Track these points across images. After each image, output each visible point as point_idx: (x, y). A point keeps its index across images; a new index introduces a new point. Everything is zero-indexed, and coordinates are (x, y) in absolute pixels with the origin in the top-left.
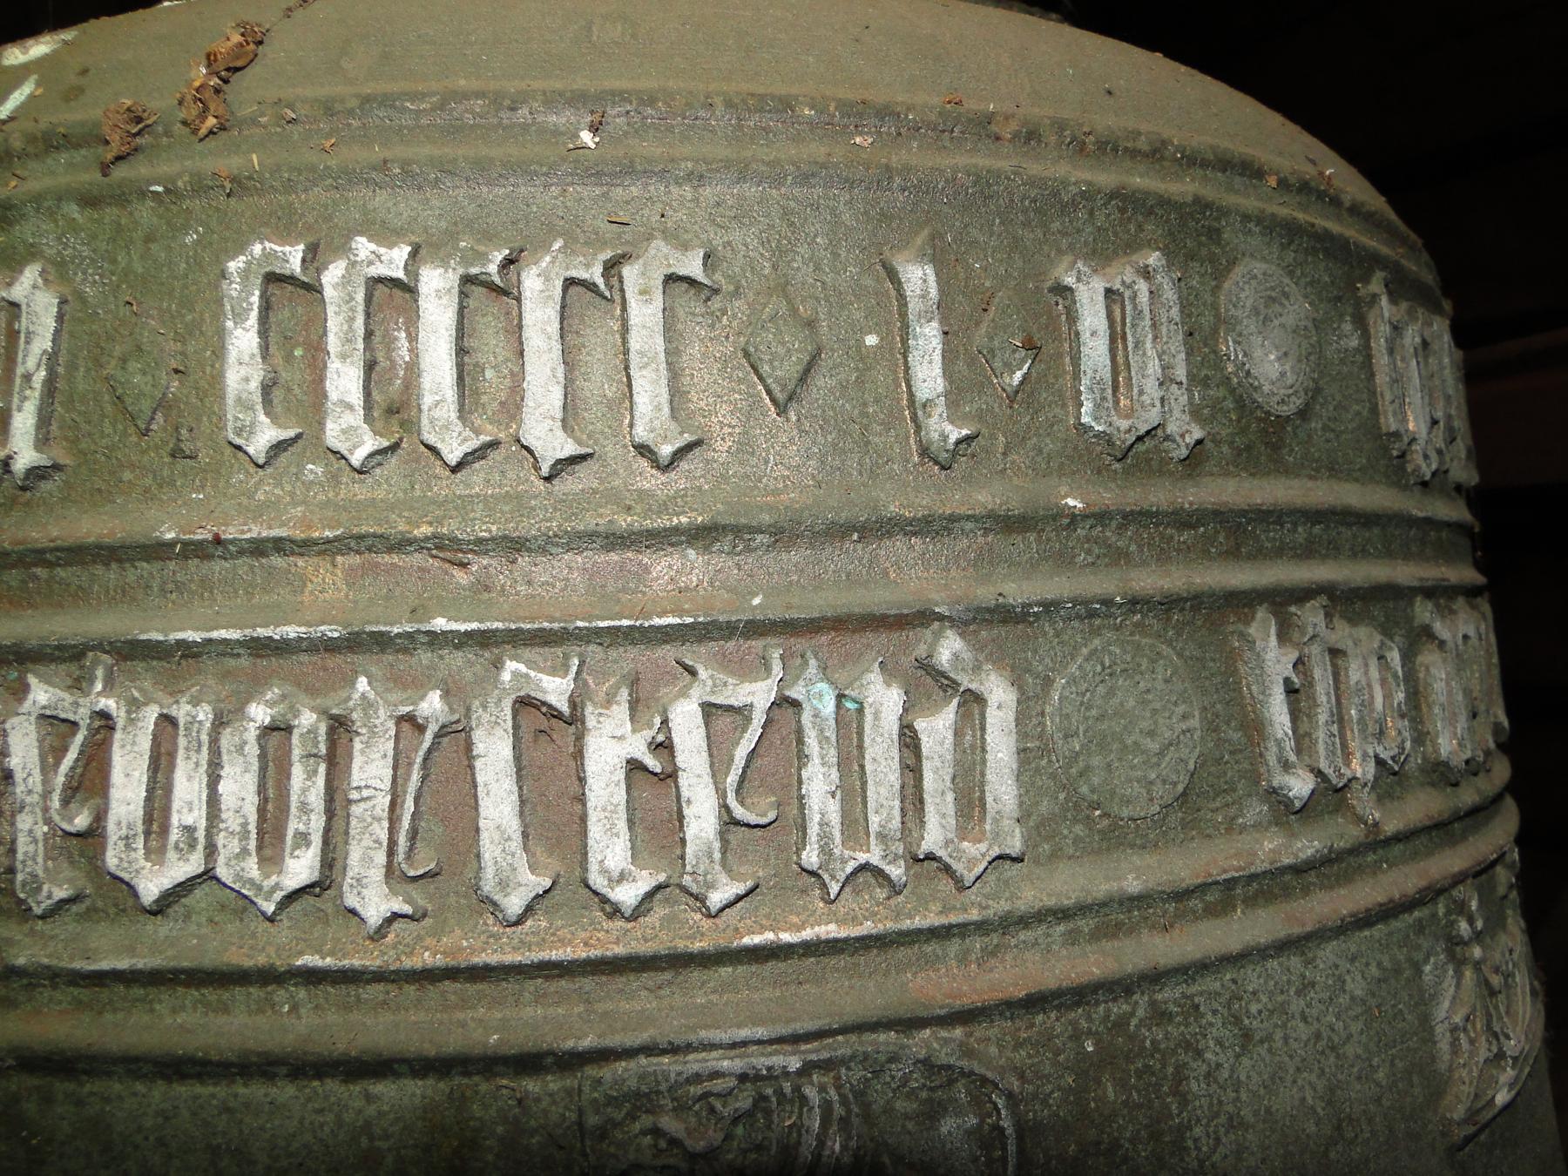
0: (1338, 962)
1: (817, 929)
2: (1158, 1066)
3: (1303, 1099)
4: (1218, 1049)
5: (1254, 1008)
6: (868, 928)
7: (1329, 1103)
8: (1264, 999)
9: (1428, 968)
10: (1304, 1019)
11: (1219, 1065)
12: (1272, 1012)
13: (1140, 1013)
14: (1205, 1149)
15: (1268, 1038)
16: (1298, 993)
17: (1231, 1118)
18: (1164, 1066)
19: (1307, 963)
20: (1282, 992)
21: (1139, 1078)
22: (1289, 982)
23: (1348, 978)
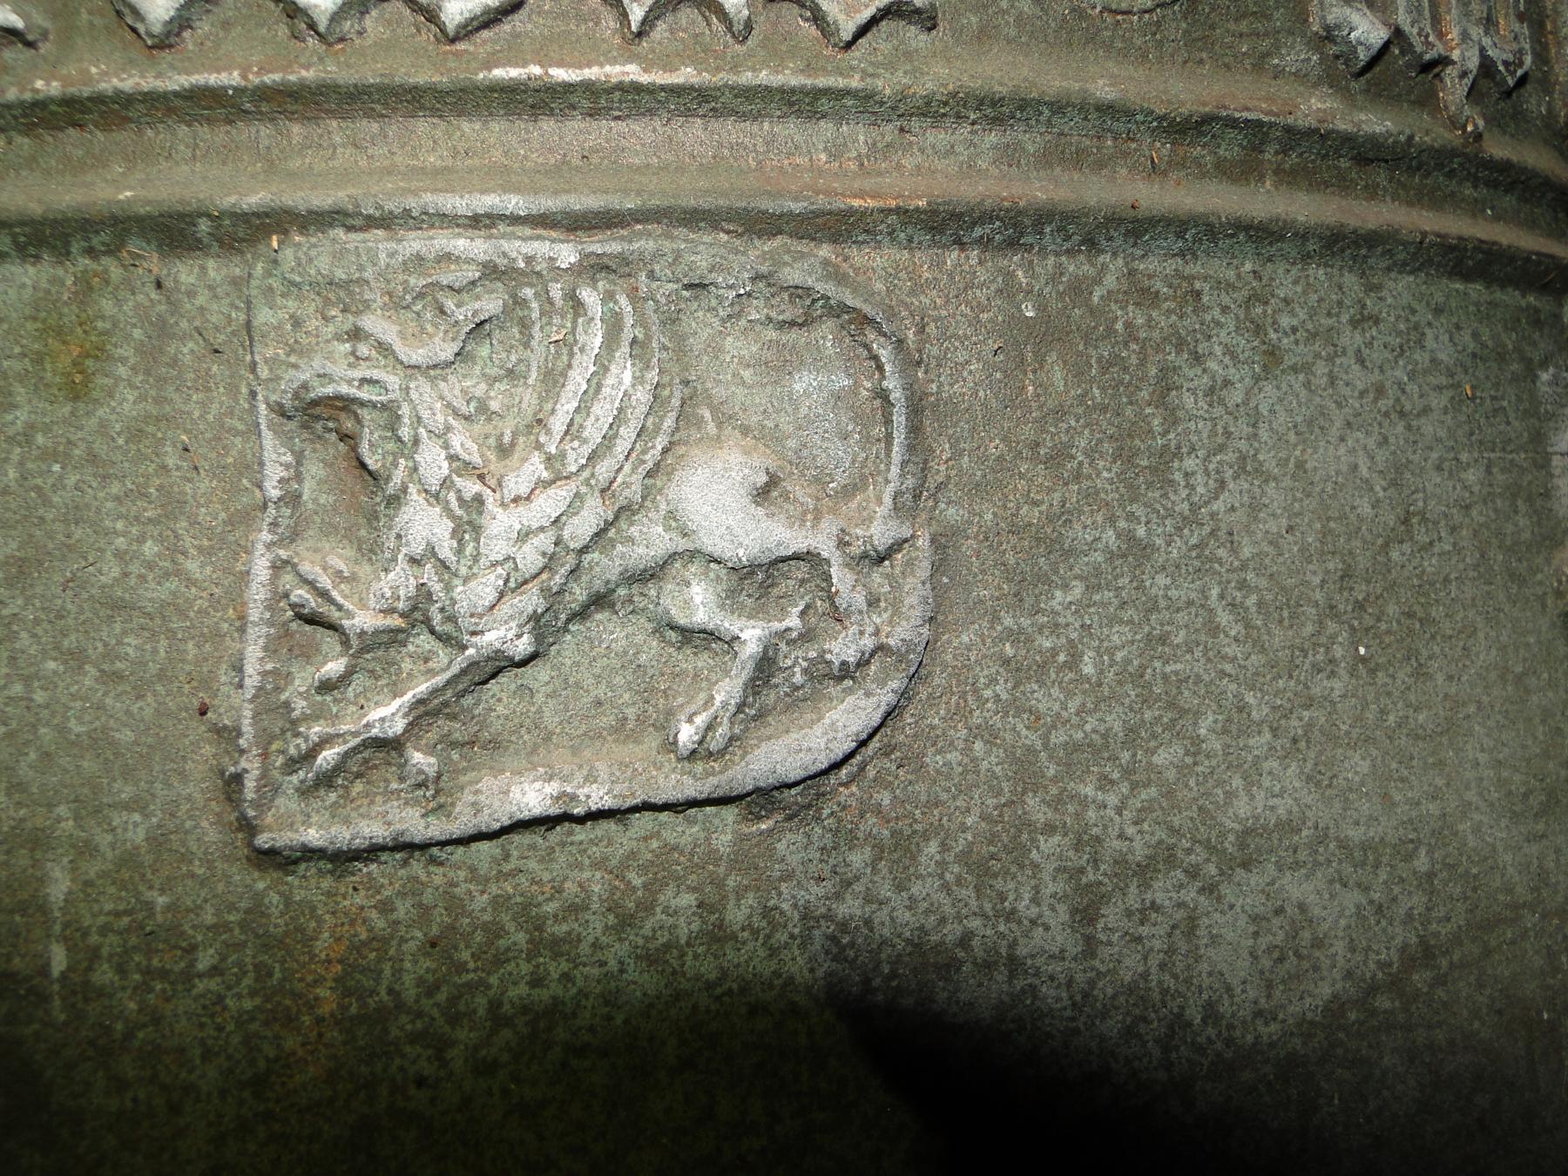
0: (1415, 305)
1: (608, 68)
2: (1134, 360)
3: (1355, 468)
4: (1227, 360)
5: (1285, 321)
6: (686, 75)
7: (1394, 483)
8: (1302, 315)
9: (1545, 376)
10: (1361, 361)
11: (1227, 383)
12: (1314, 336)
13: (1110, 281)
14: (1200, 490)
15: (1306, 368)
16: (1355, 323)
17: (1243, 458)
18: (1143, 362)
19: (1371, 288)
20: (1329, 314)
21: (1104, 370)
22: (1340, 303)
23: (1428, 331)
